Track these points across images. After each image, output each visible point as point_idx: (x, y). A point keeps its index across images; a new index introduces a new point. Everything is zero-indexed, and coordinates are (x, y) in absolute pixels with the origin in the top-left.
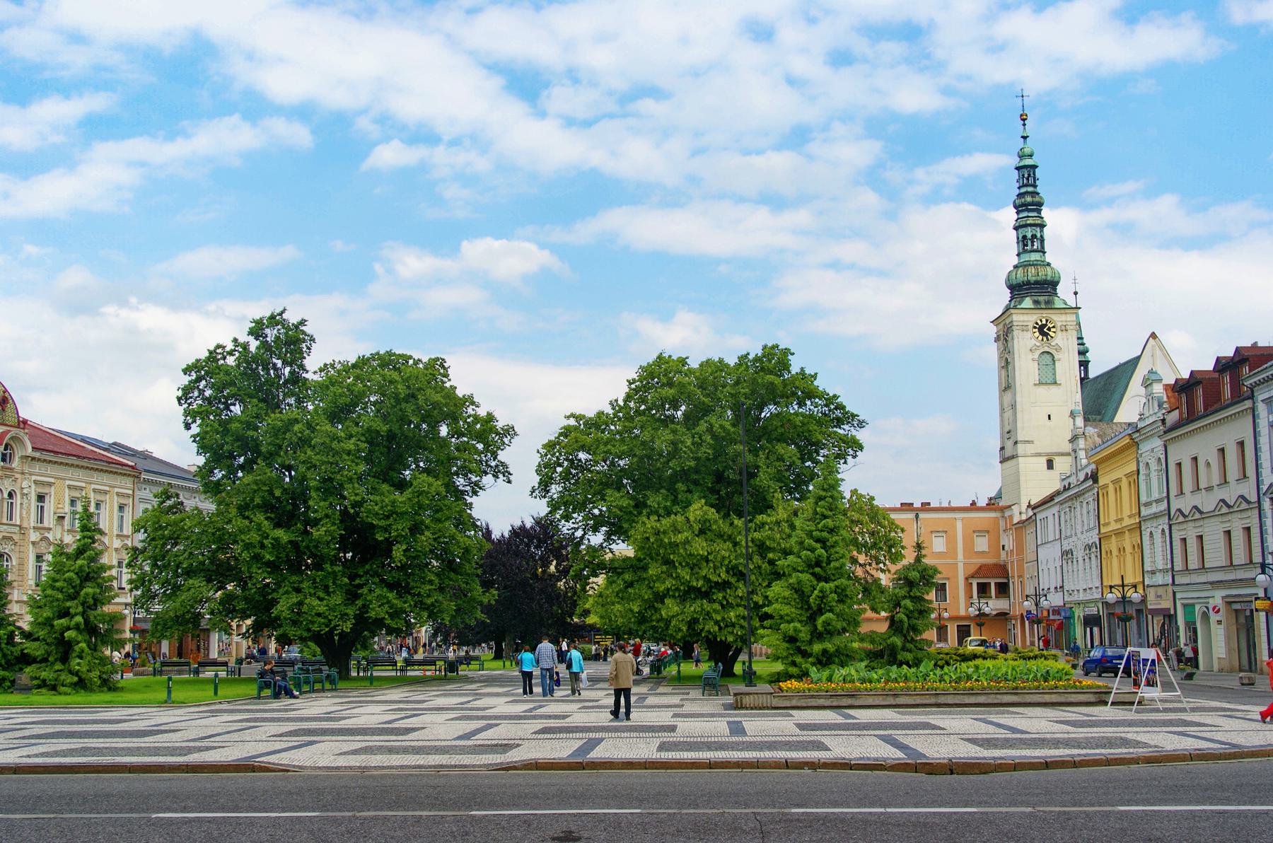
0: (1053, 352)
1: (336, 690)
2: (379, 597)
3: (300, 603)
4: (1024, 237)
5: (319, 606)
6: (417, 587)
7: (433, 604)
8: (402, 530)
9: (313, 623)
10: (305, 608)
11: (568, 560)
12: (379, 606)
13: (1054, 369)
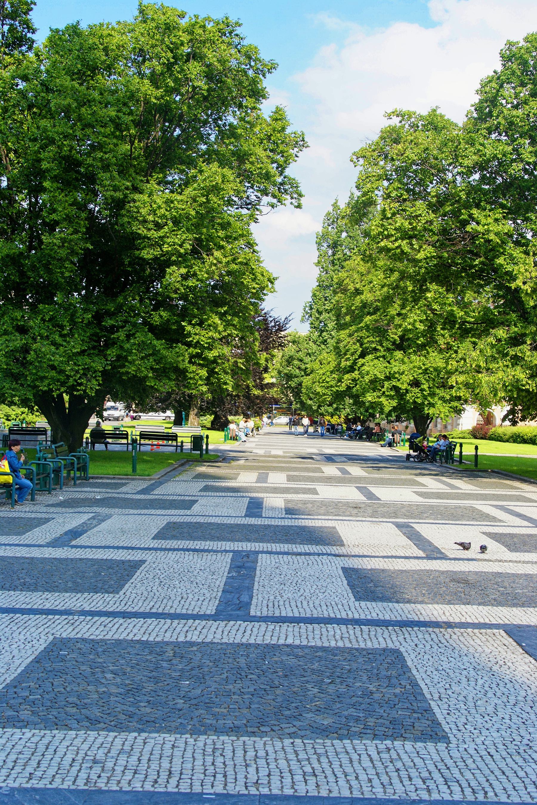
1: (86, 478)
2: (142, 346)
3: (26, 350)
5: (53, 354)
6: (196, 334)
7: (215, 361)
8: (181, 246)
9: (42, 379)
10: (31, 357)
11: (86, 390)
12: (142, 358)
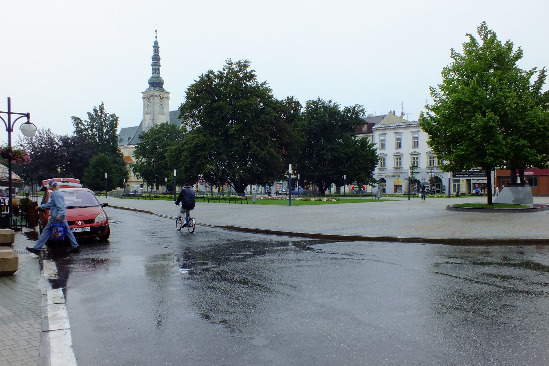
0: (163, 105)
4: (155, 69)
13: (163, 110)
